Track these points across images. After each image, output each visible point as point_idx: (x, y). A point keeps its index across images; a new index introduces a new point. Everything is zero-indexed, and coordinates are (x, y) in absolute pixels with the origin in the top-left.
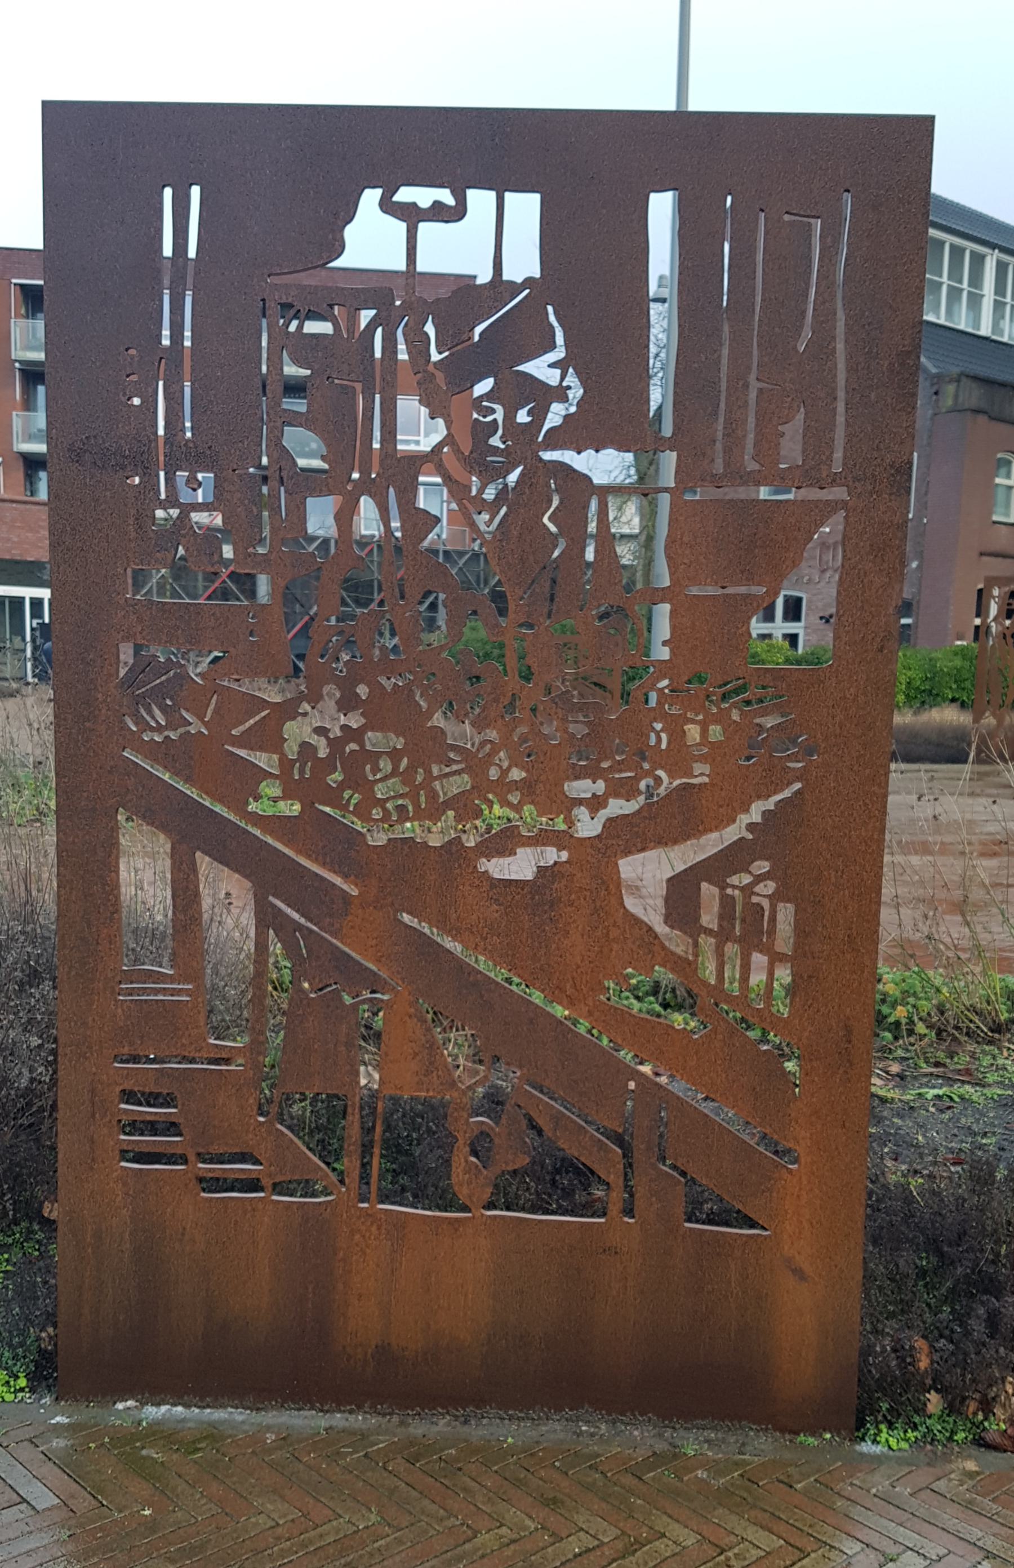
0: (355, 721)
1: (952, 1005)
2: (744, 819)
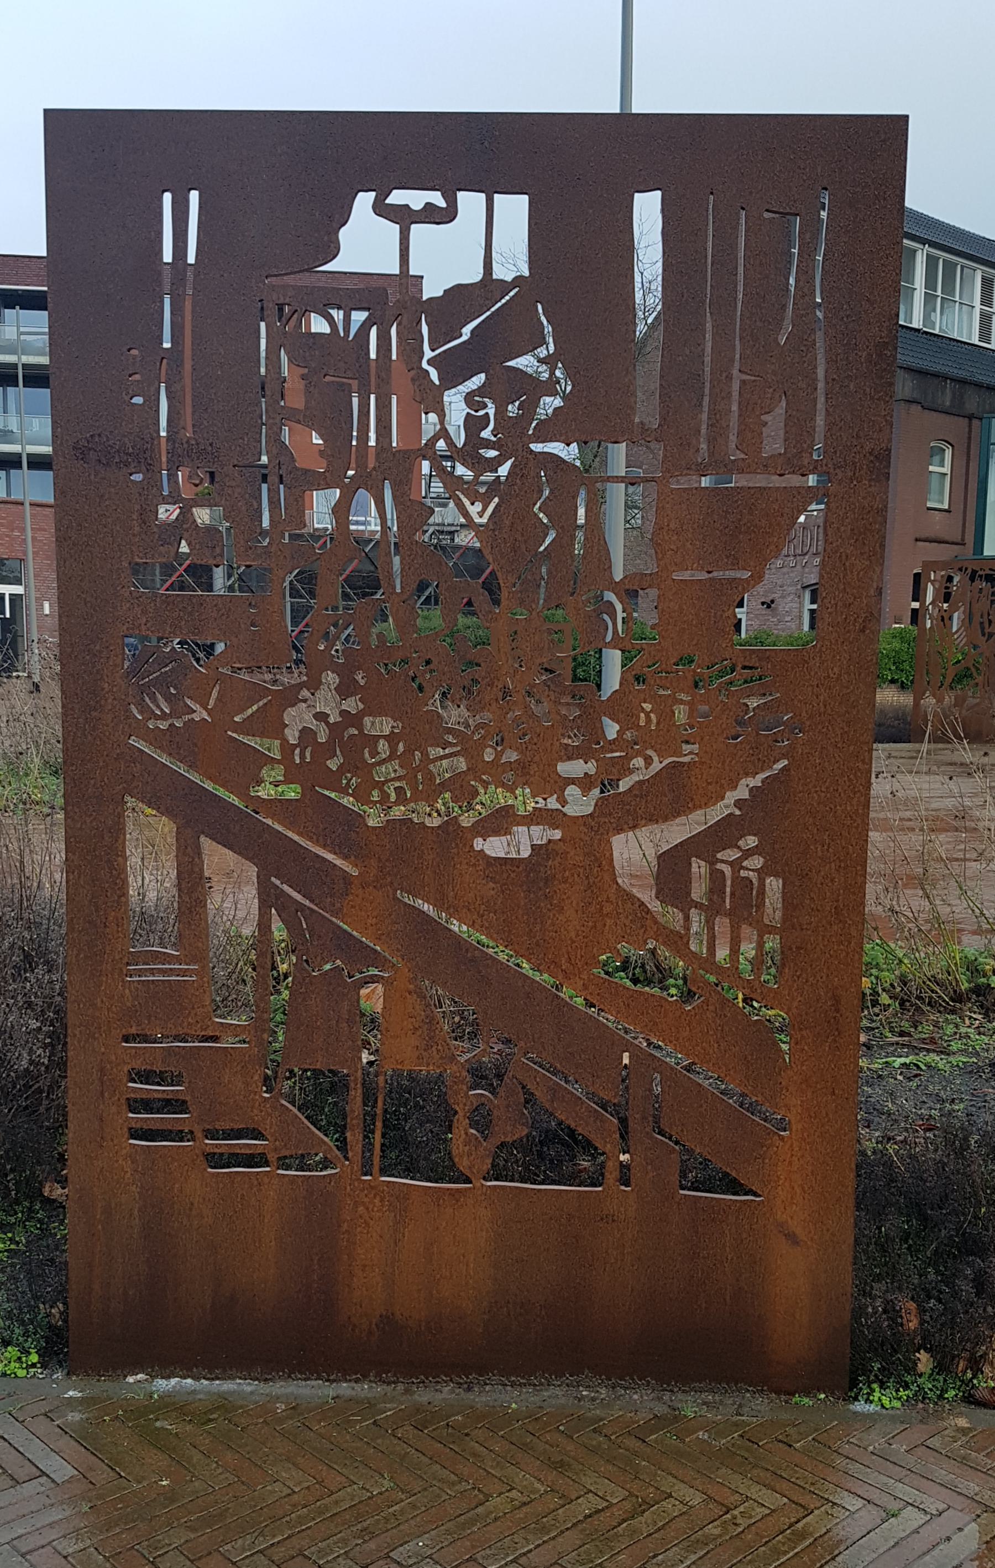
0: (352, 705)
1: (914, 975)
2: (731, 797)
